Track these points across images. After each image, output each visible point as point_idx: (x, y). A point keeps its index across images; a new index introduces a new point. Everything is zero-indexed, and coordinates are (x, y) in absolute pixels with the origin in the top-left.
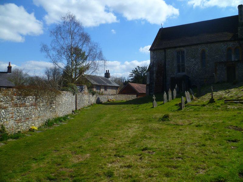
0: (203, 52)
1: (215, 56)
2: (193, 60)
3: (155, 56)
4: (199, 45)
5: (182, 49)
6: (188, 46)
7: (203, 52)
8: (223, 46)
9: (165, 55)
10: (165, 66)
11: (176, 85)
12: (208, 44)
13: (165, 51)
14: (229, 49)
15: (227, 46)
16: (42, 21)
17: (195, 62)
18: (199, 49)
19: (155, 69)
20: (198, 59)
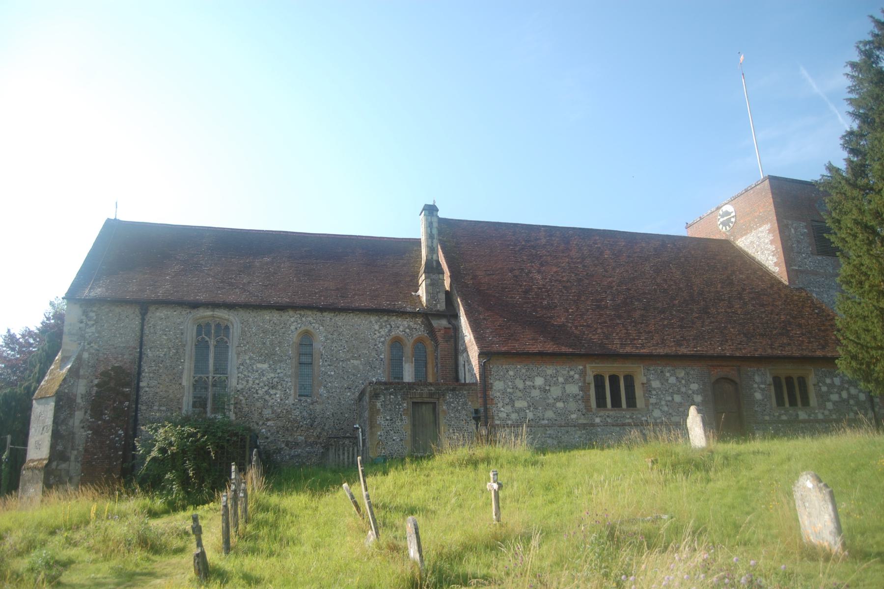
0: (307, 339)
1: (349, 360)
2: (265, 366)
3: (93, 329)
4: (291, 313)
5: (222, 314)
6: (246, 306)
7: (307, 339)
8: (377, 327)
9: (142, 330)
10: (139, 381)
11: (424, 299)
12: (325, 314)
13: (144, 314)
14: (397, 343)
15: (390, 331)
16: (435, 257)
17: (273, 375)
18: (293, 328)
19: (81, 388)
20: (283, 365)
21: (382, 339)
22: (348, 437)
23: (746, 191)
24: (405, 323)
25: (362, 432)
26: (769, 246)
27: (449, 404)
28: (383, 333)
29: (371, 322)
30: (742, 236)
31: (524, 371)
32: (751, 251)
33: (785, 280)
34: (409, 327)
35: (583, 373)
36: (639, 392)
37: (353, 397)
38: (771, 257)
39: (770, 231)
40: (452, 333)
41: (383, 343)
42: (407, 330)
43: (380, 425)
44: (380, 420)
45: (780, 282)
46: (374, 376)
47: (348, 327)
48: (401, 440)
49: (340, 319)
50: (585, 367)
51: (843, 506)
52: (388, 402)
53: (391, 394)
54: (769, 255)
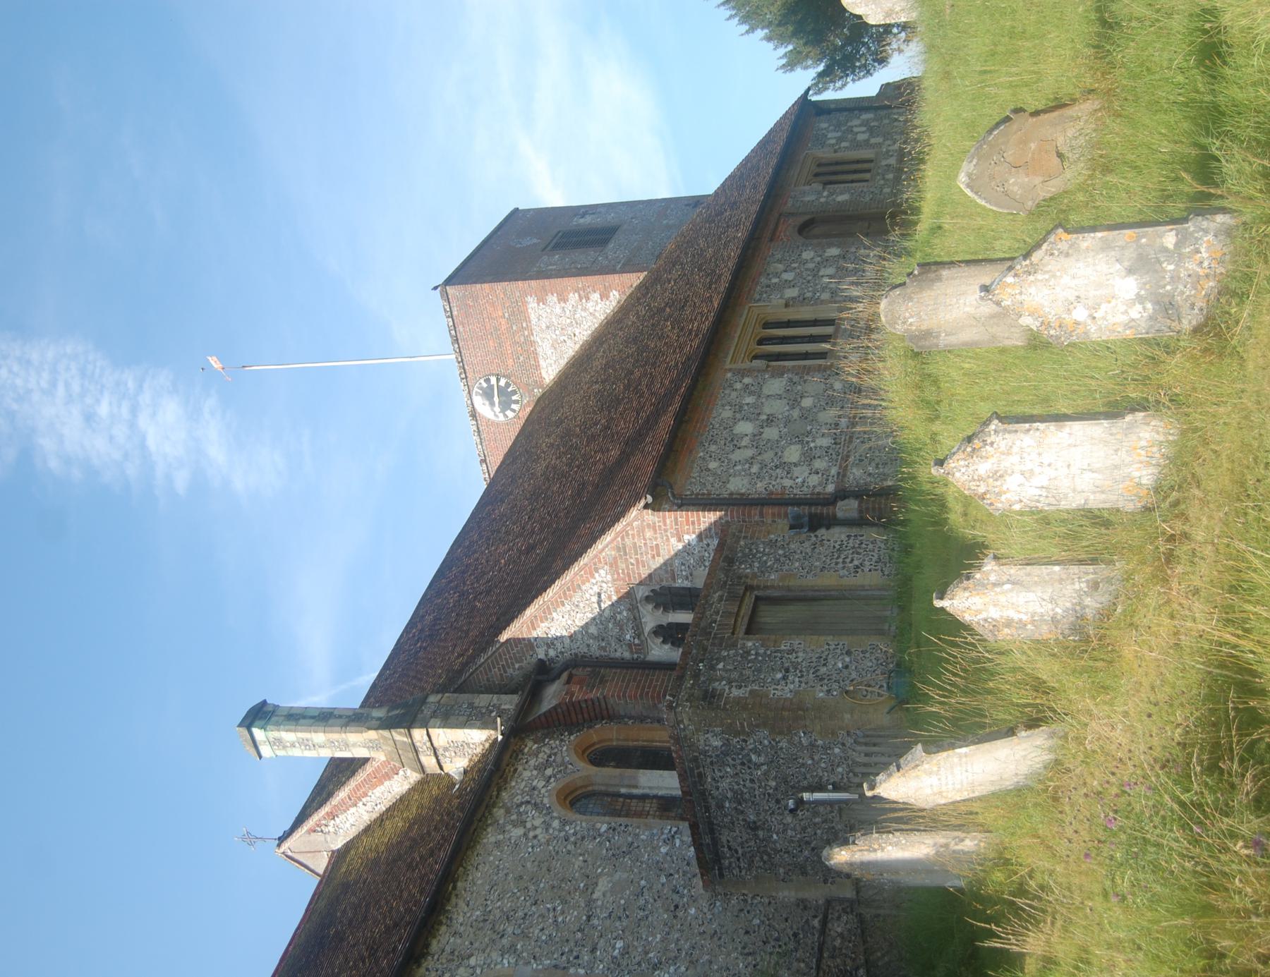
1: (590, 903)
12: (435, 946)
21: (556, 824)
22: (824, 923)
23: (456, 340)
24: (527, 774)
25: (812, 789)
26: (569, 306)
27: (764, 568)
28: (537, 822)
29: (498, 844)
30: (538, 367)
31: (713, 448)
32: (571, 349)
33: (635, 279)
34: (541, 768)
35: (742, 373)
36: (806, 313)
37: (704, 904)
38: (590, 305)
39: (541, 300)
40: (579, 672)
41: (564, 823)
42: (549, 772)
43: (797, 693)
44: (785, 691)
45: (639, 287)
46: (656, 849)
47: (494, 896)
48: (849, 653)
49: (464, 910)
50: (730, 370)
51: (978, 804)
52: (735, 675)
53: (713, 668)
54: (585, 309)
